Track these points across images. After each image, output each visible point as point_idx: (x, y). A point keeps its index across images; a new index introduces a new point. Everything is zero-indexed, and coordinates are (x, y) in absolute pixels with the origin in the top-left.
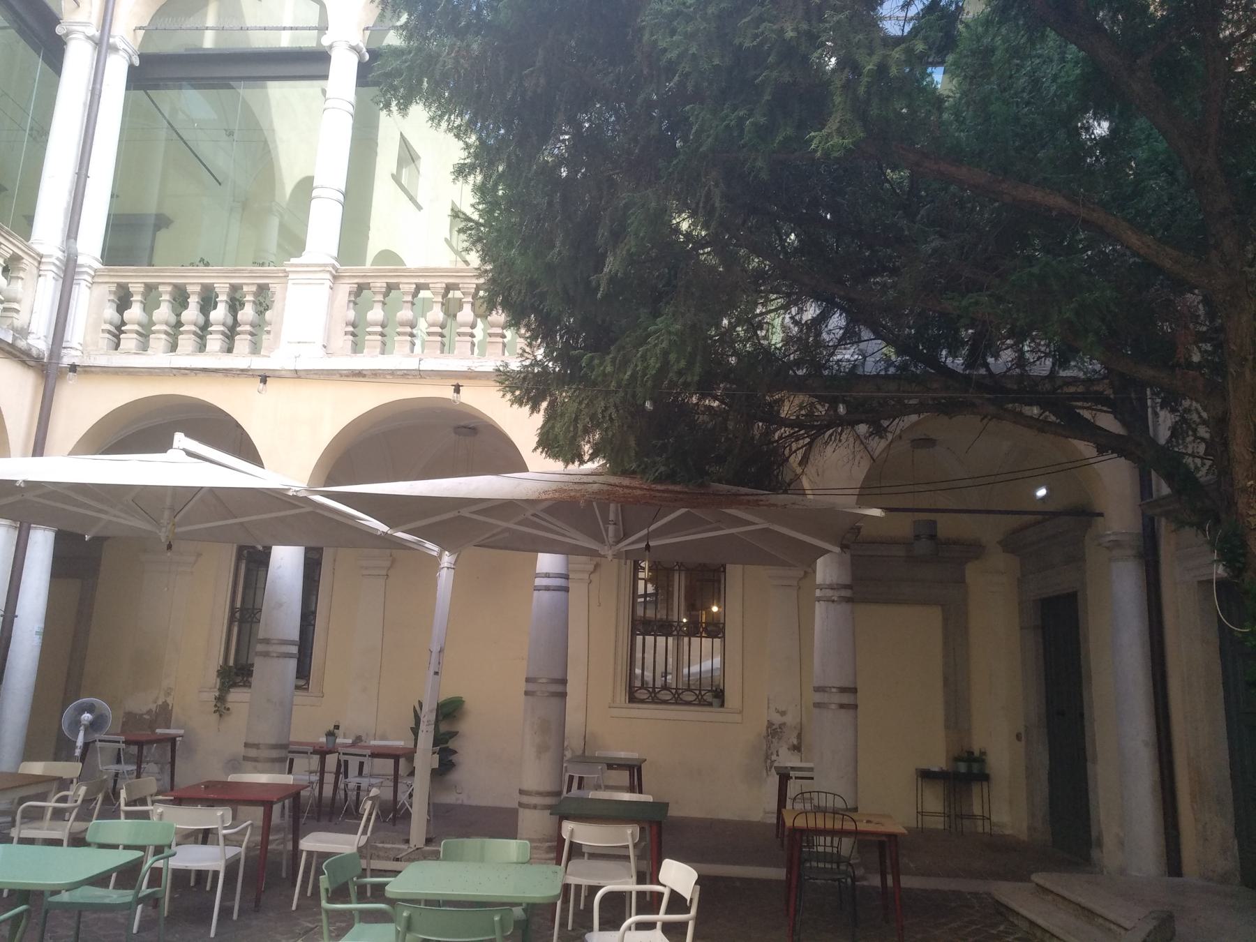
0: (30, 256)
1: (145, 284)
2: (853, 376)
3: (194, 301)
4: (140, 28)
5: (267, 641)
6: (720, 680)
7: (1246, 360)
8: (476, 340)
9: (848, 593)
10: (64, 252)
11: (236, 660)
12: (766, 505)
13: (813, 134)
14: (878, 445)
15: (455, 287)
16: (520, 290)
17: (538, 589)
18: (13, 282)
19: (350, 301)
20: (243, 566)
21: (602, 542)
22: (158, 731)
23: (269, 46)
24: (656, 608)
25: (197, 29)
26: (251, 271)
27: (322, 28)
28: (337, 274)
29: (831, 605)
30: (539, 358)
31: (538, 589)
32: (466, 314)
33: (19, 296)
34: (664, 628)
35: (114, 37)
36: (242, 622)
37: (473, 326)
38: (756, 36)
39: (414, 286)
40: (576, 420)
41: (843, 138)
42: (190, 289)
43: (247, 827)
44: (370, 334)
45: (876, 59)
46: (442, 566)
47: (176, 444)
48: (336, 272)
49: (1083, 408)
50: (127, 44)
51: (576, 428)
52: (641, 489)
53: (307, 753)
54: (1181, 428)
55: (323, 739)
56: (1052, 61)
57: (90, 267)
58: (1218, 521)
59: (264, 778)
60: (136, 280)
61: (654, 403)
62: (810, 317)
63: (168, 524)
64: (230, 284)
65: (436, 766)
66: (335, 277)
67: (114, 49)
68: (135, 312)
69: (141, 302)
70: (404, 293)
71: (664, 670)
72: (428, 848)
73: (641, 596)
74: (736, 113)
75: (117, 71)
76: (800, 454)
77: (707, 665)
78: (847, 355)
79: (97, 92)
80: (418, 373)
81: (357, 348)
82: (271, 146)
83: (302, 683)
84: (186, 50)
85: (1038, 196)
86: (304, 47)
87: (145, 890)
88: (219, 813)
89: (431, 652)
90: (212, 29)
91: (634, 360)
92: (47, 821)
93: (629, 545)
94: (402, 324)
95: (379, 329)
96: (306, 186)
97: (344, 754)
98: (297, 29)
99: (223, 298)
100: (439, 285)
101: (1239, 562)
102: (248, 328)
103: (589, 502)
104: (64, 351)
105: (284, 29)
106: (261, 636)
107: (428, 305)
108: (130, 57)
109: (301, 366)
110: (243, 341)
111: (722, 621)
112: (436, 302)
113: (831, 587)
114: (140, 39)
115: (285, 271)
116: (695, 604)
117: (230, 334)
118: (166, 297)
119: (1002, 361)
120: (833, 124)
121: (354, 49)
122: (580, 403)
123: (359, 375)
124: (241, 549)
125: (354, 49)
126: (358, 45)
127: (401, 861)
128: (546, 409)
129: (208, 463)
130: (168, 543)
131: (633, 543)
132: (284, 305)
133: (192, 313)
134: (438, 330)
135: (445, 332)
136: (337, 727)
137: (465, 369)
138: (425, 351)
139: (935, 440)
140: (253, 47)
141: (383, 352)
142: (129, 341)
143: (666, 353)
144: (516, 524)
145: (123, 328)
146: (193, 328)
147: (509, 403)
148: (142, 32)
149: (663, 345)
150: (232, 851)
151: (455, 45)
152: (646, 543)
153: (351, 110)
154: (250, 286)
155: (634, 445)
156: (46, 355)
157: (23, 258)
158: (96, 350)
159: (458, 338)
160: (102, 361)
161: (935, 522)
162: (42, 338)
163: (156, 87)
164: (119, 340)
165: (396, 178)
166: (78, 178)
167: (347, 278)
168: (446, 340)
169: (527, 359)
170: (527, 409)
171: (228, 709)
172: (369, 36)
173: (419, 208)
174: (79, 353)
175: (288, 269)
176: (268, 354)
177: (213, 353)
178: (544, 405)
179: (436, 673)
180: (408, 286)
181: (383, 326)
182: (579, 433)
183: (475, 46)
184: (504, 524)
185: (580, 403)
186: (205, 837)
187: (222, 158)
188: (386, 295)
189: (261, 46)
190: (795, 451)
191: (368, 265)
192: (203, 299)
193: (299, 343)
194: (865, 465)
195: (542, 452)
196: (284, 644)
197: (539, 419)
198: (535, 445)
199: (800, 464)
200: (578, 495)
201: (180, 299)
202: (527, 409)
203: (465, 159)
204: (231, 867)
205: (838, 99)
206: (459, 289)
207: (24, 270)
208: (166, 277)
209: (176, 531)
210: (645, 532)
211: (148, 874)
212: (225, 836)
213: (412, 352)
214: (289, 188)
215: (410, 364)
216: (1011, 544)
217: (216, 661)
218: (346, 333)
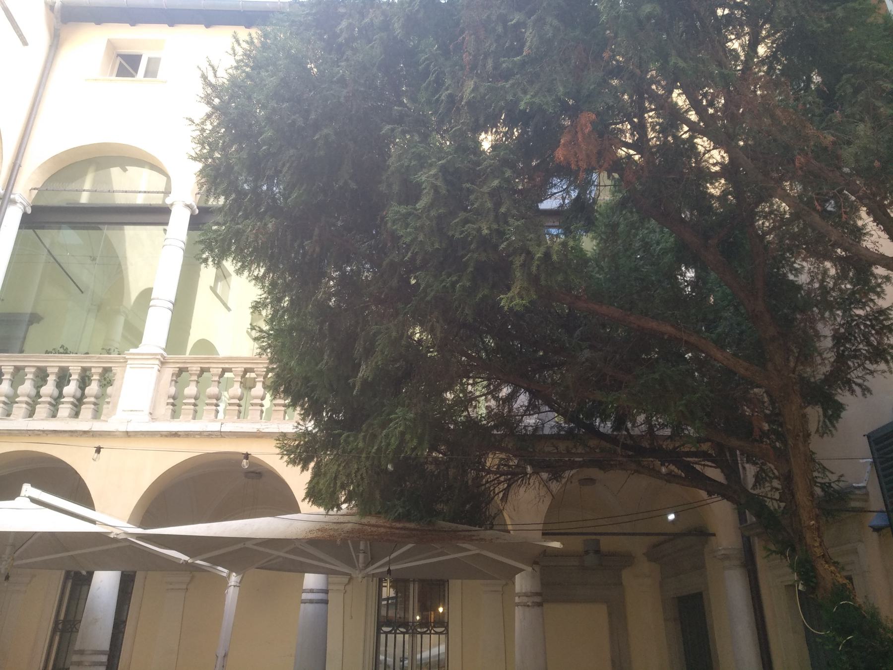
1: (15, 366)
2: (536, 436)
3: (51, 380)
4: (35, 189)
5: (82, 652)
6: (445, 663)
7: (799, 436)
8: (264, 409)
9: (538, 599)
12: (477, 540)
13: (502, 296)
14: (555, 486)
15: (251, 370)
16: (297, 383)
17: (304, 602)
19: (172, 380)
20: (57, 638)
21: (353, 566)
23: (128, 203)
24: (396, 609)
25: (77, 190)
26: (99, 358)
27: (167, 192)
29: (527, 609)
31: (304, 602)
32: (258, 390)
34: (401, 624)
35: (14, 194)
36: (63, 632)
37: (263, 398)
38: (462, 232)
39: (221, 370)
40: (336, 478)
41: (522, 300)
42: (49, 370)
45: (543, 249)
46: (230, 584)
47: (23, 493)
48: (164, 359)
49: (696, 463)
50: (24, 199)
51: (335, 484)
52: (384, 527)
54: (762, 476)
56: (655, 232)
58: (794, 550)
61: (394, 466)
62: (504, 394)
63: (8, 558)
66: (163, 363)
67: (14, 202)
69: (10, 380)
70: (213, 375)
71: (402, 656)
73: (384, 600)
74: (450, 278)
76: (501, 495)
77: (435, 651)
78: (531, 421)
80: (219, 433)
81: (175, 415)
82: (123, 267)
84: (67, 204)
85: (653, 325)
89: (217, 657)
90: (87, 191)
91: (380, 437)
93: (376, 568)
94: (210, 397)
95: (193, 401)
96: (146, 295)
98: (149, 192)
99: (75, 377)
100: (239, 369)
101: (812, 582)
102: (93, 399)
103: (344, 541)
106: (77, 648)
107: (230, 383)
108: (25, 208)
109: (131, 428)
111: (446, 621)
112: (236, 381)
113: (526, 595)
114: (33, 196)
116: (426, 606)
118: (30, 376)
119: (639, 424)
120: (515, 290)
122: (339, 465)
123: (175, 435)
124: (68, 573)
125: (189, 206)
126: (191, 204)
128: (313, 468)
129: (47, 510)
130: (6, 574)
131: (377, 568)
132: (122, 383)
133: (49, 388)
134: (237, 401)
135: (242, 403)
137: (255, 430)
138: (226, 417)
139: (595, 480)
140: (117, 203)
141: (194, 418)
143: (403, 434)
144: (287, 552)
146: (49, 399)
147: (286, 464)
148: (36, 191)
149: (401, 429)
151: (256, 224)
152: (388, 568)
153: (183, 246)
154: (97, 369)
155: (379, 498)
159: (251, 408)
161: (598, 541)
163: (43, 228)
165: (213, 289)
167: (171, 364)
168: (242, 409)
170: (299, 468)
172: (200, 199)
173: (229, 309)
175: (127, 357)
176: (106, 419)
177: (63, 419)
178: (312, 465)
180: (216, 370)
181: (196, 398)
182: (338, 489)
183: (270, 225)
184: (276, 553)
185: (339, 465)
187: (85, 275)
188: (200, 376)
190: (498, 494)
191: (187, 355)
192: (59, 378)
193: (131, 411)
194: (548, 500)
195: (309, 502)
196: (95, 654)
197: (307, 475)
198: (303, 496)
199: (502, 500)
200: (336, 534)
201: (41, 376)
202: (299, 468)
203: (261, 295)
205: (518, 274)
206: (254, 372)
208: (31, 361)
209: (14, 564)
210: (387, 559)
213: (217, 418)
215: (214, 427)
216: (653, 555)
218: (168, 404)
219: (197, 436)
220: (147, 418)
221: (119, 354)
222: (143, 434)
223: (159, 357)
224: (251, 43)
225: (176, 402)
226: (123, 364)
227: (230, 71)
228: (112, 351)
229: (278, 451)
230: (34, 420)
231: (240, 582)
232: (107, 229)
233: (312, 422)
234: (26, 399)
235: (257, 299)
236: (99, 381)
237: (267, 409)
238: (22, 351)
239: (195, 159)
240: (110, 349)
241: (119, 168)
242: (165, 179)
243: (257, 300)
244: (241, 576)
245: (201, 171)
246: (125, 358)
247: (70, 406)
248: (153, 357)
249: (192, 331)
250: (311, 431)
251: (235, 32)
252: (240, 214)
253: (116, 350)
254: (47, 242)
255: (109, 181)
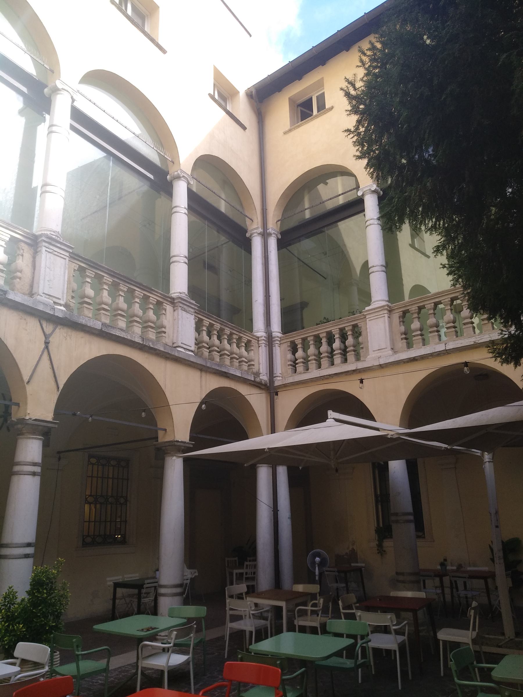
0: (254, 339)
3: (324, 341)
4: (278, 221)
5: (396, 514)
10: (266, 333)
11: (383, 524)
18: (250, 352)
19: (400, 322)
20: (380, 507)
22: (353, 564)
25: (302, 211)
26: (348, 319)
27: (358, 187)
28: (391, 309)
30: (513, 332)
32: (466, 312)
33: (253, 358)
39: (433, 304)
42: (321, 336)
43: (405, 625)
44: (415, 337)
46: (485, 461)
53: (431, 576)
55: (439, 567)
57: (278, 337)
59: (409, 594)
60: (297, 337)
64: (339, 328)
65: (511, 585)
67: (270, 234)
68: (300, 353)
69: (302, 347)
72: (517, 639)
75: (273, 243)
79: (267, 257)
81: (409, 346)
83: (420, 534)
86: (350, 200)
87: (360, 661)
88: (389, 617)
92: (309, 617)
94: (431, 327)
95: (419, 332)
96: (366, 266)
97: (453, 577)
98: (345, 193)
99: (337, 336)
100: (447, 300)
102: (352, 348)
104: (275, 378)
105: (340, 195)
107: (443, 312)
108: (277, 235)
109: (382, 362)
110: (351, 356)
112: (447, 310)
114: (279, 226)
115: (364, 315)
117: (344, 353)
118: (312, 342)
121: (374, 192)
123: (414, 360)
124: (373, 464)
127: (502, 648)
133: (324, 348)
134: (452, 324)
135: (456, 324)
136: (445, 560)
137: (472, 343)
141: (424, 345)
142: (300, 368)
145: (296, 362)
146: (326, 354)
147: (500, 364)
150: (400, 638)
156: (268, 382)
157: (251, 341)
158: (287, 375)
160: (291, 380)
162: (265, 375)
163: (290, 245)
164: (296, 368)
165: (412, 246)
166: (266, 298)
167: (396, 310)
169: (505, 335)
171: (385, 551)
174: (281, 378)
175: (365, 314)
179: (497, 527)
180: (429, 305)
183: (428, 184)
186: (385, 630)
188: (419, 313)
189: (331, 208)
191: (407, 298)
203: (440, 240)
204: (402, 646)
206: (458, 299)
207: (253, 346)
208: (310, 333)
211: (360, 649)
212: (395, 630)
213: (440, 340)
214: (358, 269)
215: (441, 347)
217: (373, 525)
218: (402, 339)
219: (430, 357)
220: (390, 352)
221: (361, 313)
222: (391, 364)
223: (386, 307)
224: (373, 48)
225: (407, 336)
226: (364, 319)
227: (364, 79)
228: (355, 312)
229: (491, 355)
230: (322, 369)
231: (493, 458)
232: (327, 230)
233: (513, 327)
234: (313, 357)
235: (437, 244)
236: (352, 334)
237: (478, 325)
238: (303, 328)
239: (359, 158)
240: (353, 312)
241: (322, 184)
242: (354, 178)
243: (438, 244)
244: (492, 453)
245: (368, 165)
246: (364, 314)
247: (340, 356)
248: (382, 309)
249: (405, 282)
250: (514, 334)
251: (359, 47)
252: (404, 184)
253: (357, 311)
254: (296, 253)
255: (319, 196)
